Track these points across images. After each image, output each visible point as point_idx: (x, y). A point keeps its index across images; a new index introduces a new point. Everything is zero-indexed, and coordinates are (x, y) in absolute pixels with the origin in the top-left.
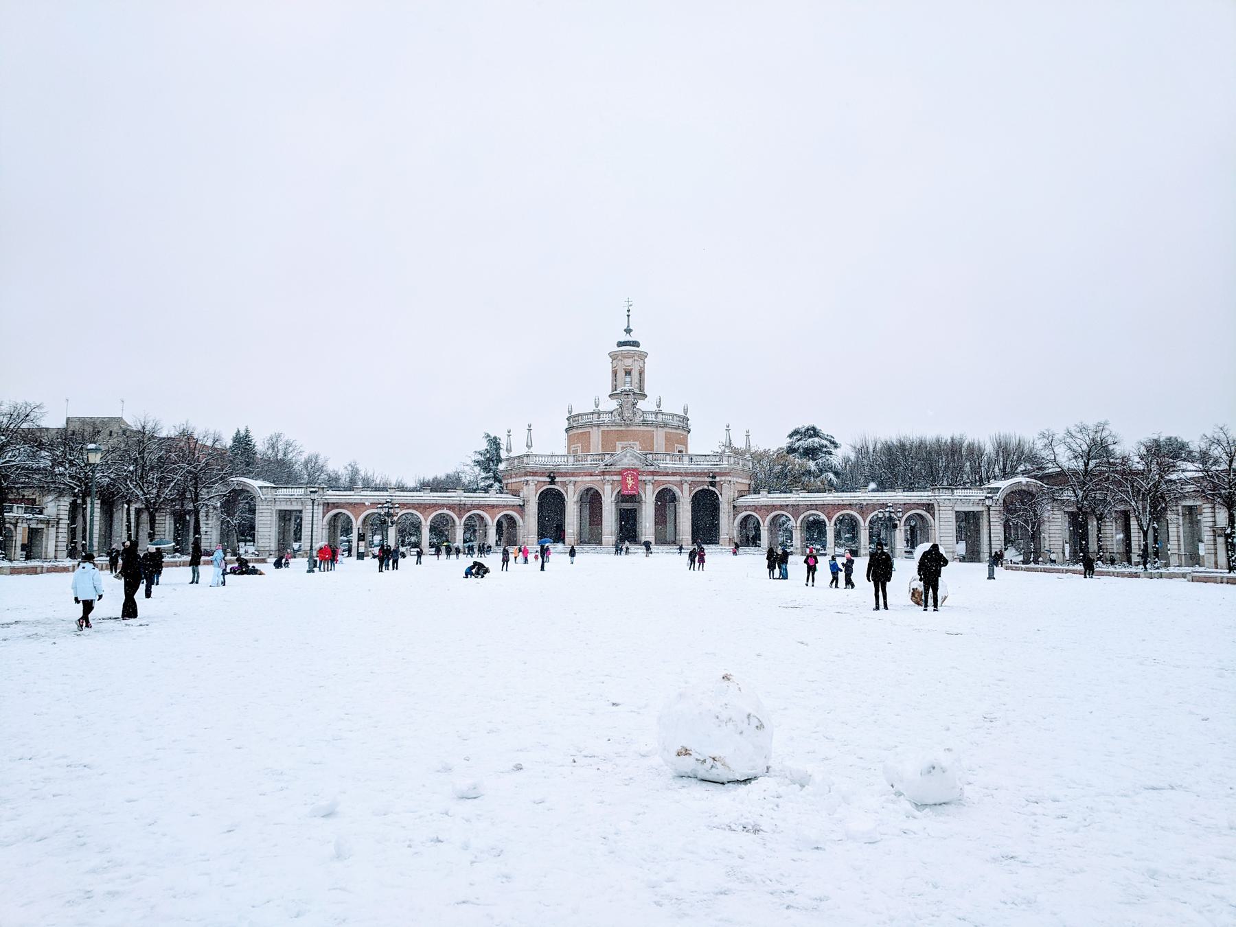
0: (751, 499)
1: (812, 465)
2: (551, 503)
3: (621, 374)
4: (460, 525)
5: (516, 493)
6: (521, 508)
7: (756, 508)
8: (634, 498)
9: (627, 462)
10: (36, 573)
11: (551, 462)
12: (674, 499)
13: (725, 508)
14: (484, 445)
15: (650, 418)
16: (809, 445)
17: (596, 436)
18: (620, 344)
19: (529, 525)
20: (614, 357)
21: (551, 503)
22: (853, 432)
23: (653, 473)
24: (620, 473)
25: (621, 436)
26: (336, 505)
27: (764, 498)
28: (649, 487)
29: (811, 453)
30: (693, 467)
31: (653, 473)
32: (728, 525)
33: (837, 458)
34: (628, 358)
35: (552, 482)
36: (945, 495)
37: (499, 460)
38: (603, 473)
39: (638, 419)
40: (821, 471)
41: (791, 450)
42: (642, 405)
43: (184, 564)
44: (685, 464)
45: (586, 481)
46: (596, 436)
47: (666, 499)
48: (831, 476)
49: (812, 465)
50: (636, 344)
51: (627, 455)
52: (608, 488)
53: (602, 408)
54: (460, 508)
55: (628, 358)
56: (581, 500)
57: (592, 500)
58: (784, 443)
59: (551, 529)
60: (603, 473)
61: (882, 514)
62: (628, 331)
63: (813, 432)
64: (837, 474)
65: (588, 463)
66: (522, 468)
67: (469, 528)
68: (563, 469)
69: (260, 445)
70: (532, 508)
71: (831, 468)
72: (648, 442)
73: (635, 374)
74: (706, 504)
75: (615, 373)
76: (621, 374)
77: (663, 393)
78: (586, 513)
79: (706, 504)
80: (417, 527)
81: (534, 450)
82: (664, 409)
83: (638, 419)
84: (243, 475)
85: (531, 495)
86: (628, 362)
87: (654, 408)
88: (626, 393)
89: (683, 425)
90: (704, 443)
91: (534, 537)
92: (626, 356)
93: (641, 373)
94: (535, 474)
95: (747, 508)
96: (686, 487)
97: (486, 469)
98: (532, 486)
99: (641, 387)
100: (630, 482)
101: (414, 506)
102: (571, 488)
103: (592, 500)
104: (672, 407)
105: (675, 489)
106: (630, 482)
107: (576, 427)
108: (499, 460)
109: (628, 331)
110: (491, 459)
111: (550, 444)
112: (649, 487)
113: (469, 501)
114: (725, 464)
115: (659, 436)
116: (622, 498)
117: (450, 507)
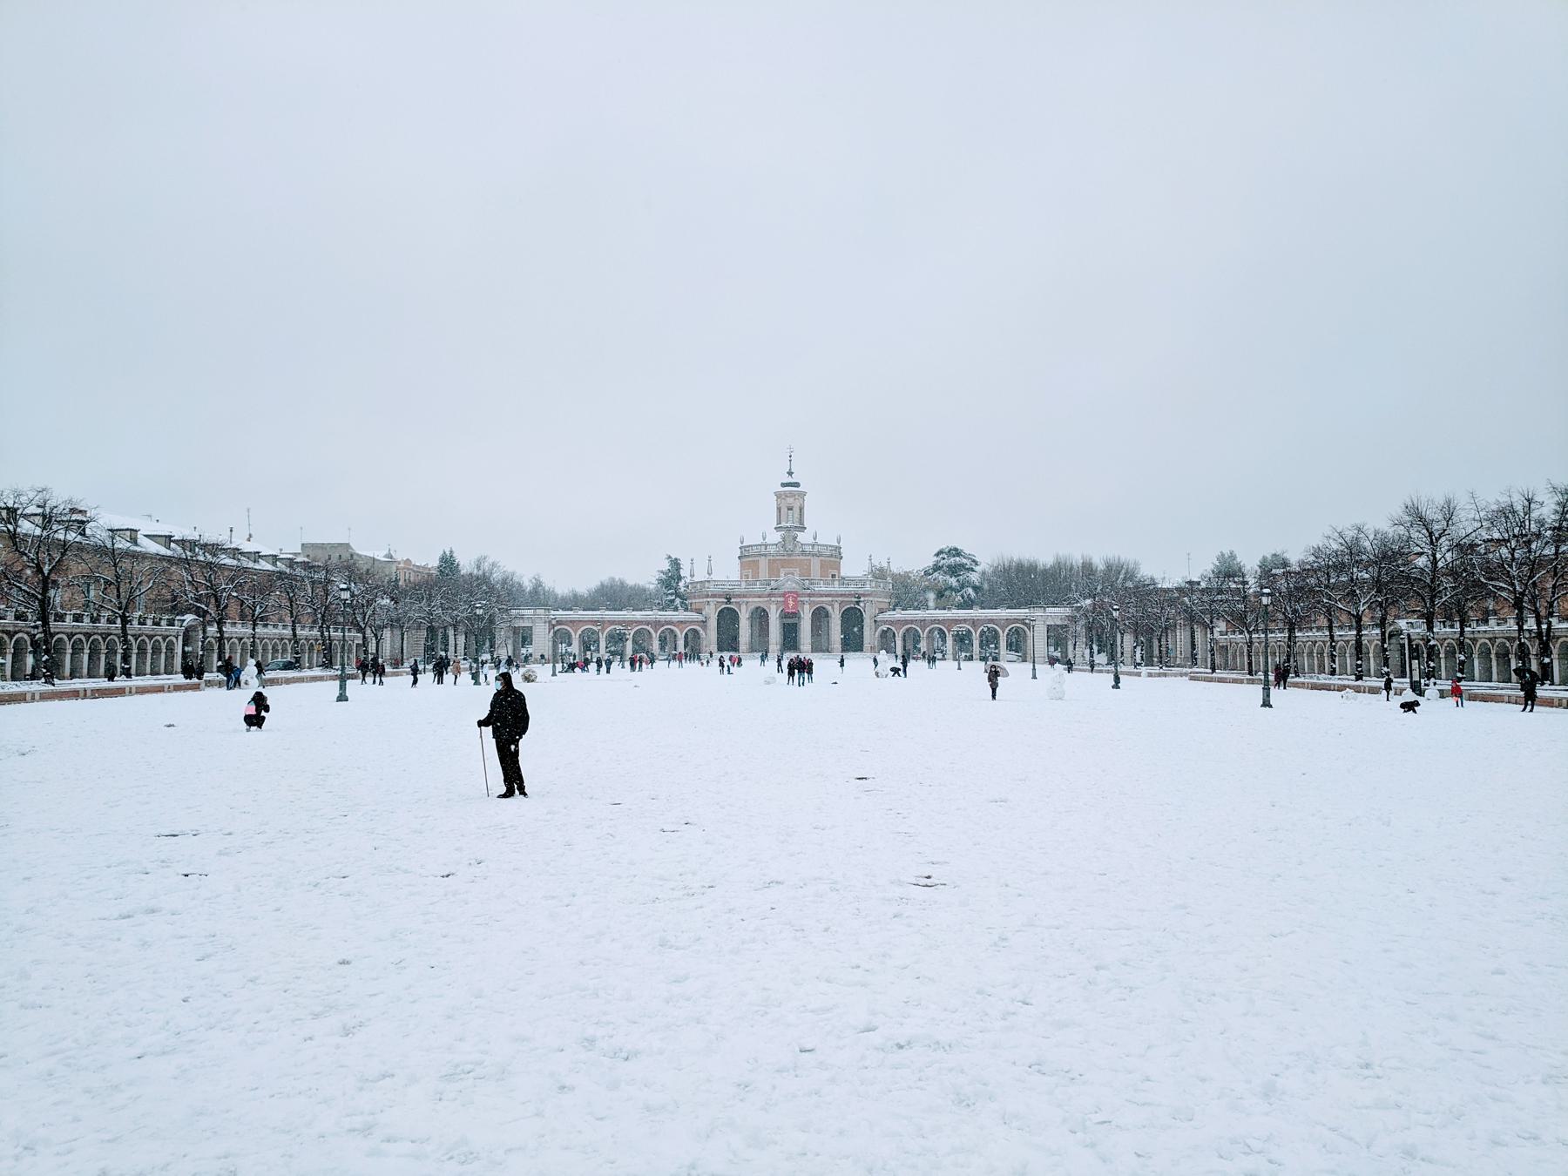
0: (888, 615)
1: (953, 581)
2: (728, 619)
3: (784, 510)
4: (655, 636)
5: (699, 611)
6: (704, 623)
7: (891, 623)
8: (796, 615)
9: (790, 586)
10: (25, 700)
11: (727, 588)
12: (827, 615)
13: (868, 622)
14: (666, 566)
15: (809, 549)
16: (953, 563)
17: (763, 563)
18: (784, 485)
19: (710, 637)
20: (778, 495)
21: (728, 619)
22: (990, 551)
23: (809, 595)
24: (783, 595)
25: (785, 563)
26: (559, 623)
27: (899, 614)
28: (807, 607)
29: (954, 570)
30: (843, 589)
31: (809, 595)
32: (870, 636)
33: (974, 577)
34: (790, 501)
35: (729, 600)
36: (1038, 613)
37: (680, 578)
38: (769, 595)
39: (798, 550)
40: (962, 587)
41: (937, 568)
42: (803, 537)
43: (332, 678)
44: (836, 587)
45: (756, 602)
46: (763, 563)
47: (820, 615)
48: (970, 591)
49: (953, 581)
50: (797, 485)
51: (789, 581)
52: (773, 607)
53: (768, 541)
54: (657, 624)
55: (790, 501)
56: (752, 618)
57: (760, 616)
58: (930, 561)
59: (728, 641)
60: (769, 595)
61: (1124, 622)
62: (790, 473)
63: (956, 552)
64: (975, 588)
65: (758, 588)
66: (701, 590)
67: (663, 640)
68: (737, 591)
69: (466, 564)
70: (713, 623)
71: (969, 584)
72: (806, 573)
73: (796, 510)
74: (853, 618)
75: (779, 509)
76: (784, 510)
77: (819, 528)
78: (756, 628)
79: (853, 618)
80: (996, 636)
81: (714, 577)
82: (819, 541)
83: (798, 550)
84: (163, 558)
85: (712, 613)
86: (790, 500)
87: (811, 541)
88: (788, 529)
89: (836, 553)
90: (854, 567)
91: (714, 647)
92: (786, 495)
93: (801, 509)
94: (714, 596)
95: (885, 622)
96: (837, 606)
97: (668, 586)
98: (712, 606)
99: (801, 520)
100: (791, 603)
101: (620, 623)
102: (743, 607)
103: (760, 616)
104: (827, 539)
105: (829, 608)
106: (791, 603)
107: (748, 556)
108: (680, 578)
109: (790, 473)
110: (672, 577)
111: (728, 571)
112: (807, 607)
113: (662, 619)
114: (868, 587)
115: (816, 564)
116: (784, 615)
117: (648, 623)
